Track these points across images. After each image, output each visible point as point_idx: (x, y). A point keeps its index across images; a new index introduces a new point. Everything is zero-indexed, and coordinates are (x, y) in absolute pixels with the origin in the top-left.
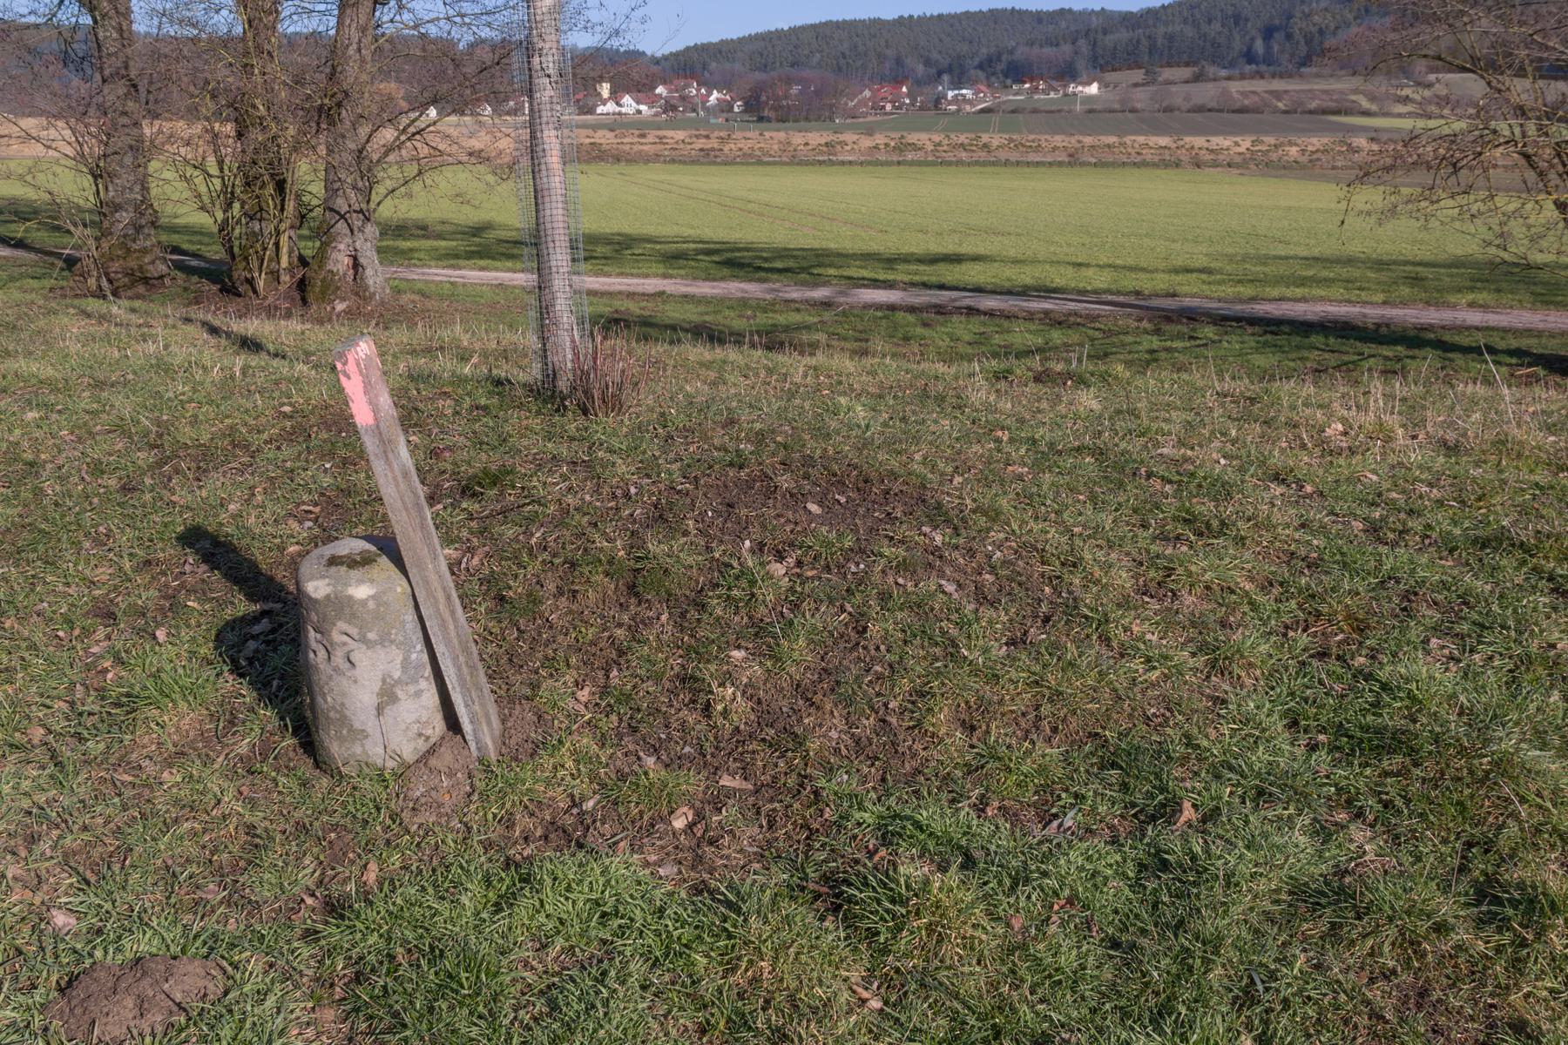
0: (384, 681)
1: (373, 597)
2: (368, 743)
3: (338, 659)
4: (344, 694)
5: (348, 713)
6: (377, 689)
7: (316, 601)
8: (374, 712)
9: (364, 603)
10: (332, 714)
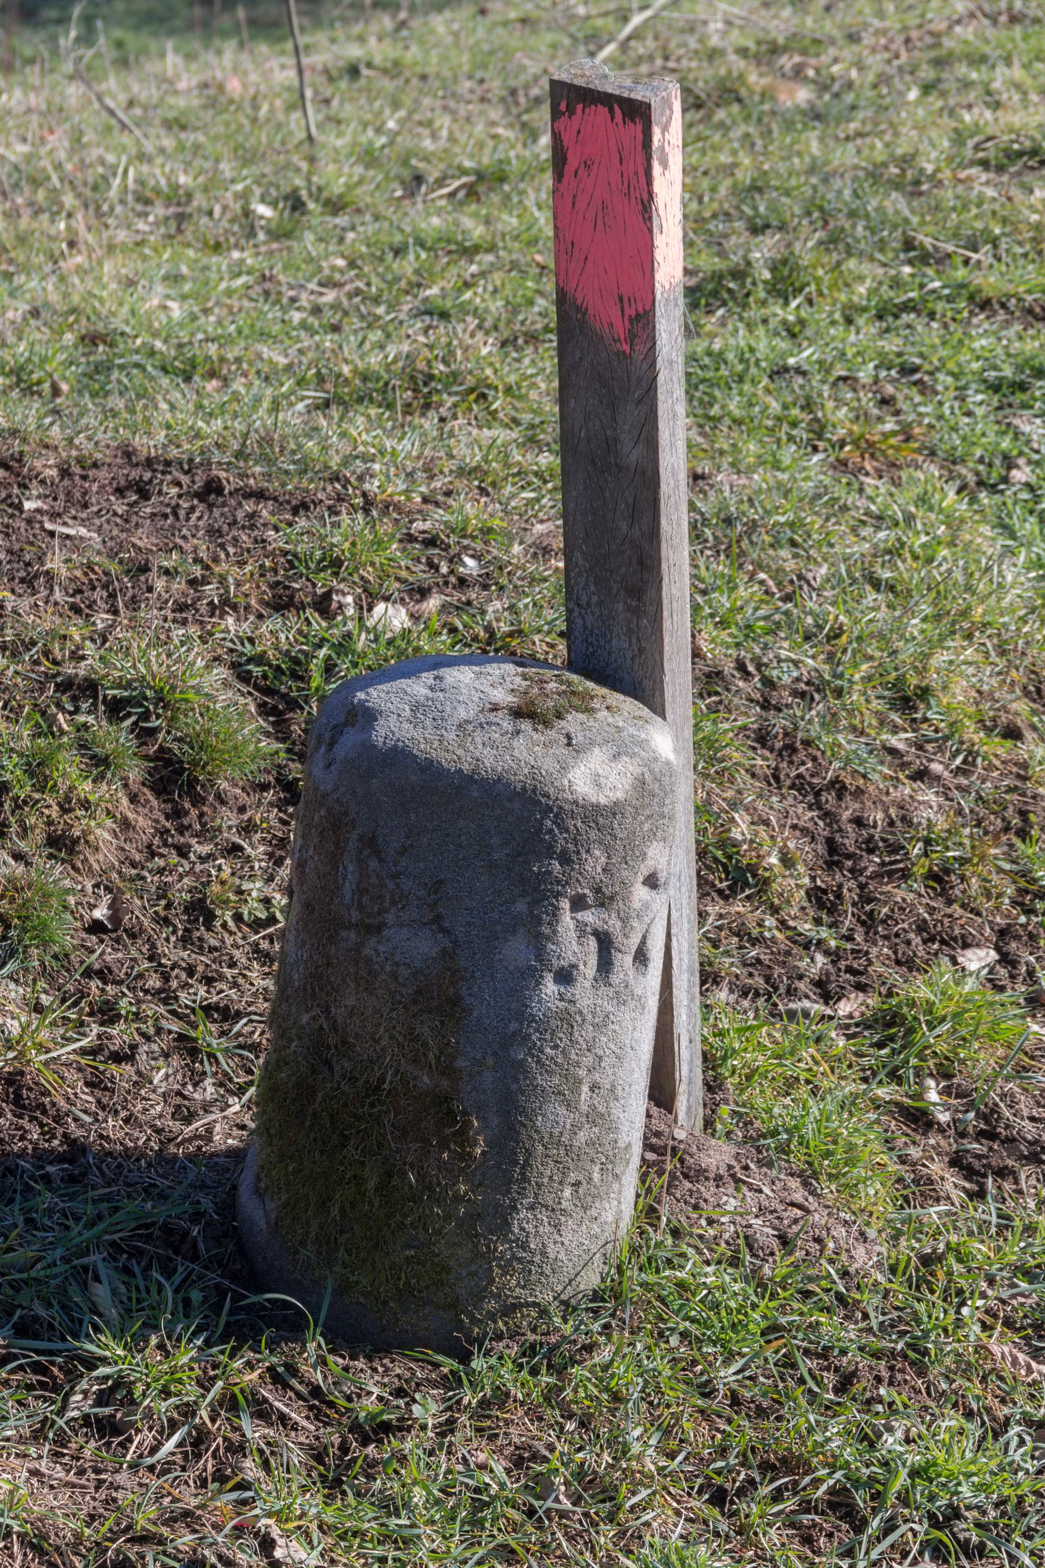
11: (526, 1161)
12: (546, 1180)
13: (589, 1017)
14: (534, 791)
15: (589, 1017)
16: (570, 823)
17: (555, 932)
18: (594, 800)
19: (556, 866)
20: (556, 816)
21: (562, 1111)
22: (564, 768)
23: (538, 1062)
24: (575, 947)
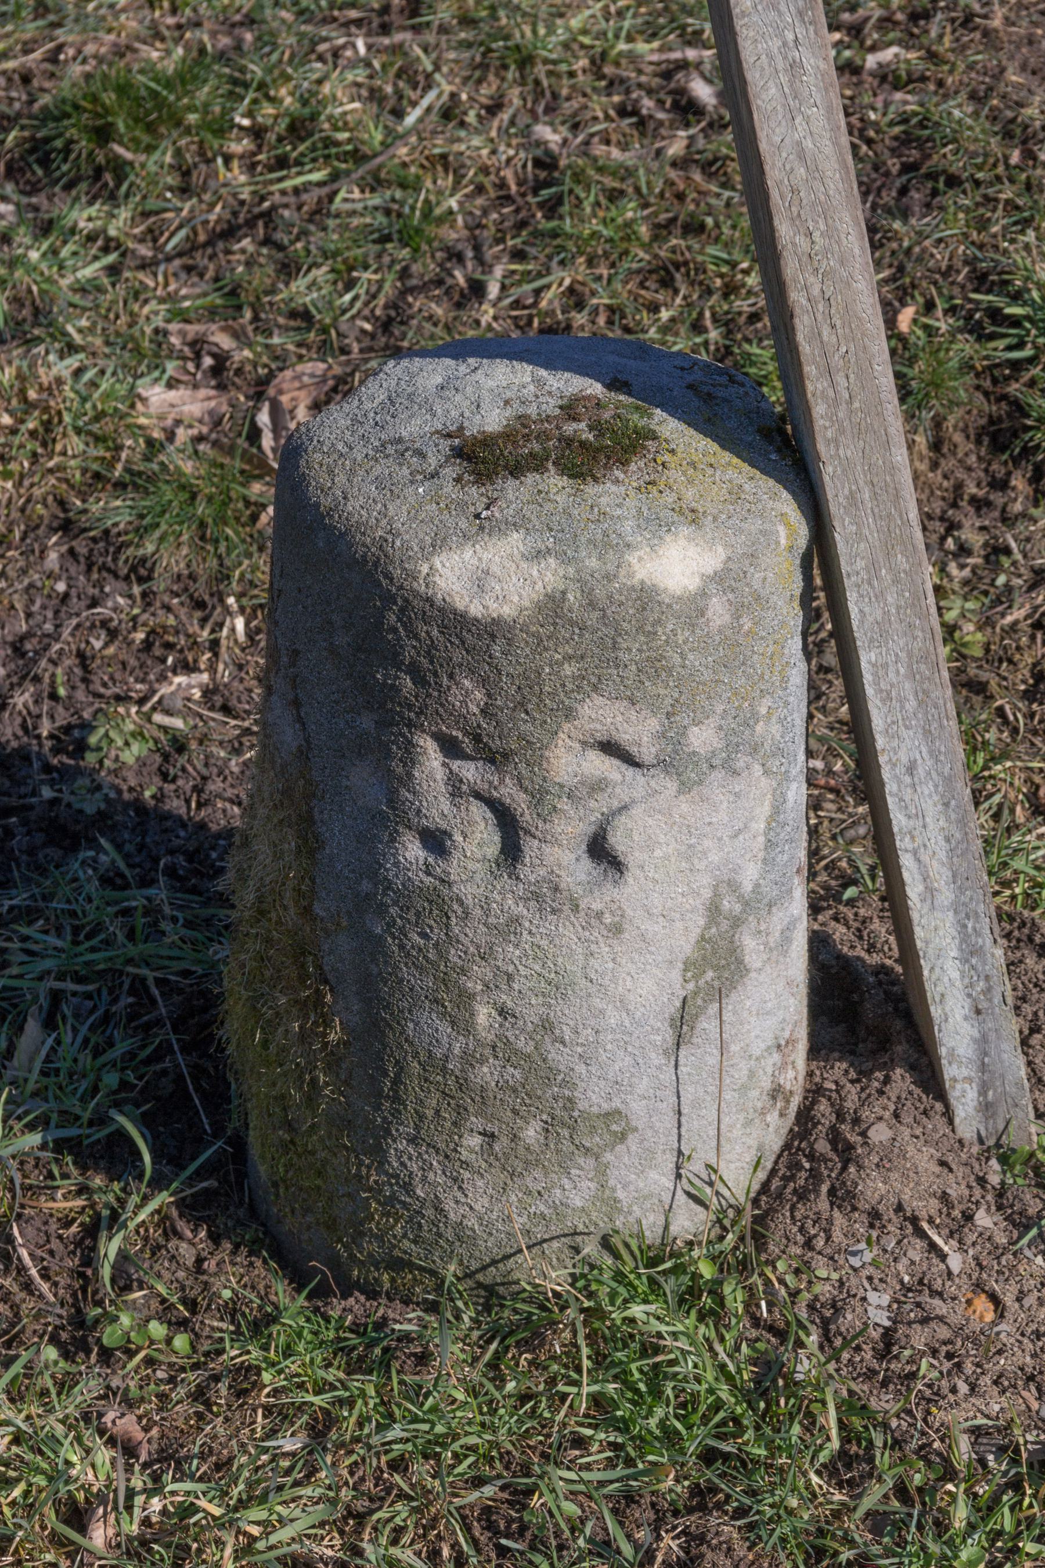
0: (714, 910)
1: (720, 579)
2: (622, 1162)
3: (559, 853)
4: (558, 987)
5: (558, 1056)
6: (685, 945)
7: (493, 629)
8: (665, 1036)
9: (694, 607)
10: (486, 1074)
11: (398, 1075)
12: (429, 1113)
13: (478, 912)
14: (376, 564)
15: (478, 912)
16: (422, 629)
17: (410, 776)
18: (460, 605)
19: (407, 683)
20: (402, 610)
21: (445, 1028)
22: (439, 544)
23: (402, 947)
24: (445, 805)
